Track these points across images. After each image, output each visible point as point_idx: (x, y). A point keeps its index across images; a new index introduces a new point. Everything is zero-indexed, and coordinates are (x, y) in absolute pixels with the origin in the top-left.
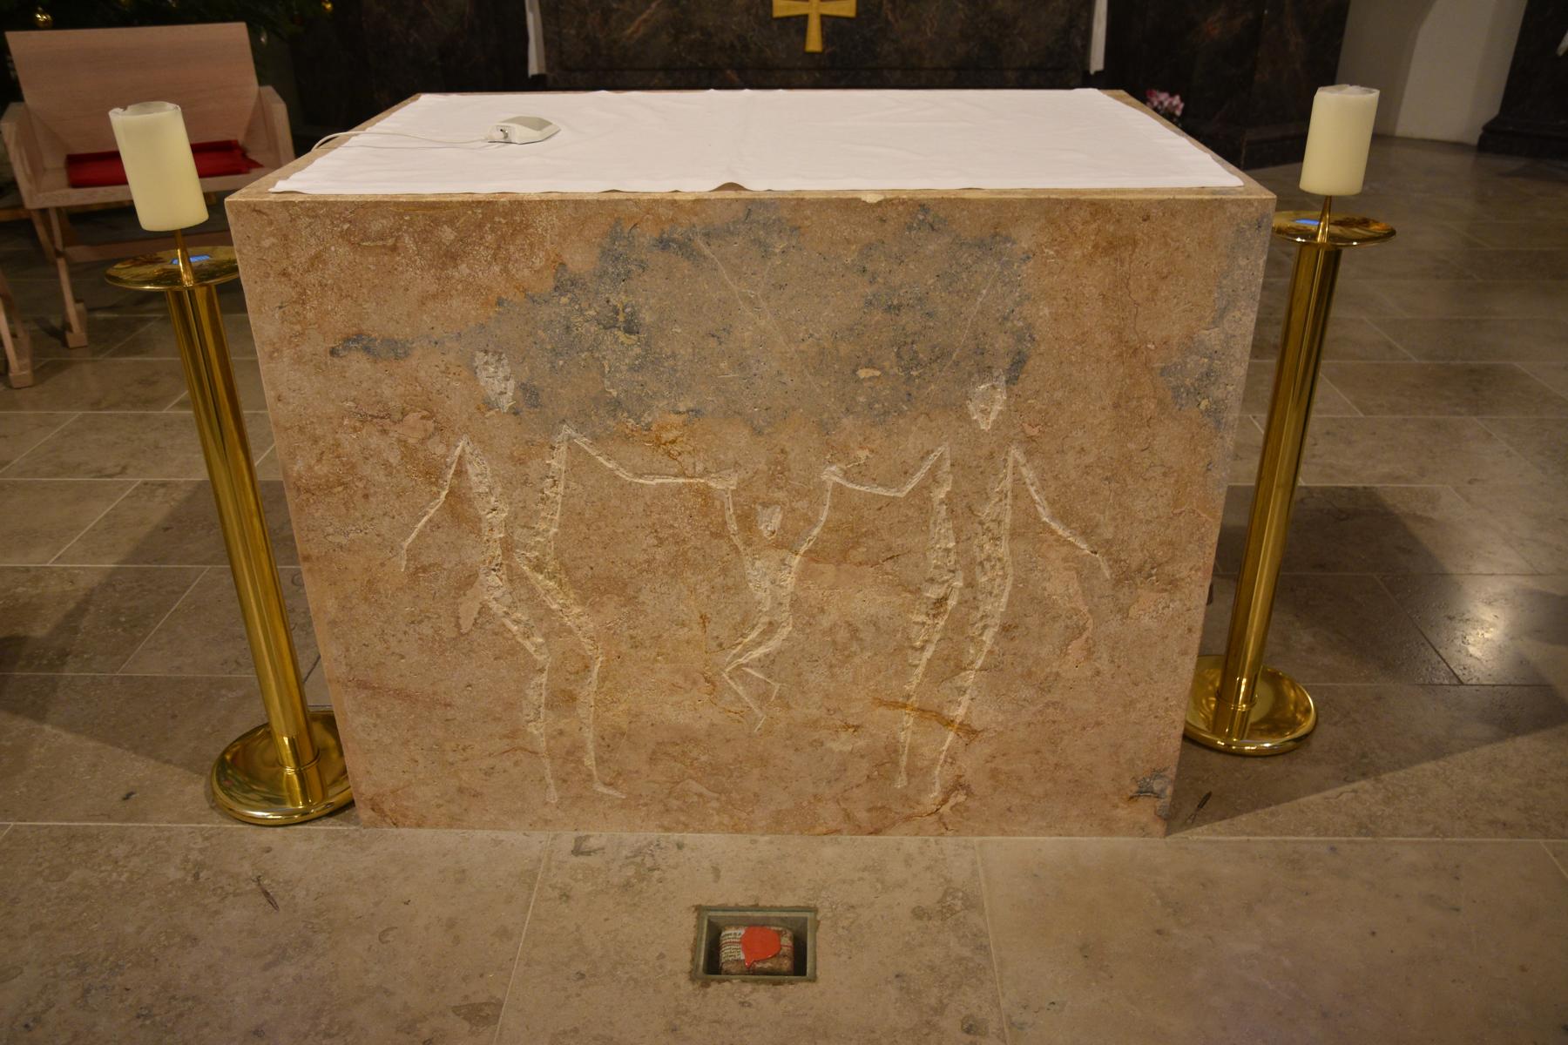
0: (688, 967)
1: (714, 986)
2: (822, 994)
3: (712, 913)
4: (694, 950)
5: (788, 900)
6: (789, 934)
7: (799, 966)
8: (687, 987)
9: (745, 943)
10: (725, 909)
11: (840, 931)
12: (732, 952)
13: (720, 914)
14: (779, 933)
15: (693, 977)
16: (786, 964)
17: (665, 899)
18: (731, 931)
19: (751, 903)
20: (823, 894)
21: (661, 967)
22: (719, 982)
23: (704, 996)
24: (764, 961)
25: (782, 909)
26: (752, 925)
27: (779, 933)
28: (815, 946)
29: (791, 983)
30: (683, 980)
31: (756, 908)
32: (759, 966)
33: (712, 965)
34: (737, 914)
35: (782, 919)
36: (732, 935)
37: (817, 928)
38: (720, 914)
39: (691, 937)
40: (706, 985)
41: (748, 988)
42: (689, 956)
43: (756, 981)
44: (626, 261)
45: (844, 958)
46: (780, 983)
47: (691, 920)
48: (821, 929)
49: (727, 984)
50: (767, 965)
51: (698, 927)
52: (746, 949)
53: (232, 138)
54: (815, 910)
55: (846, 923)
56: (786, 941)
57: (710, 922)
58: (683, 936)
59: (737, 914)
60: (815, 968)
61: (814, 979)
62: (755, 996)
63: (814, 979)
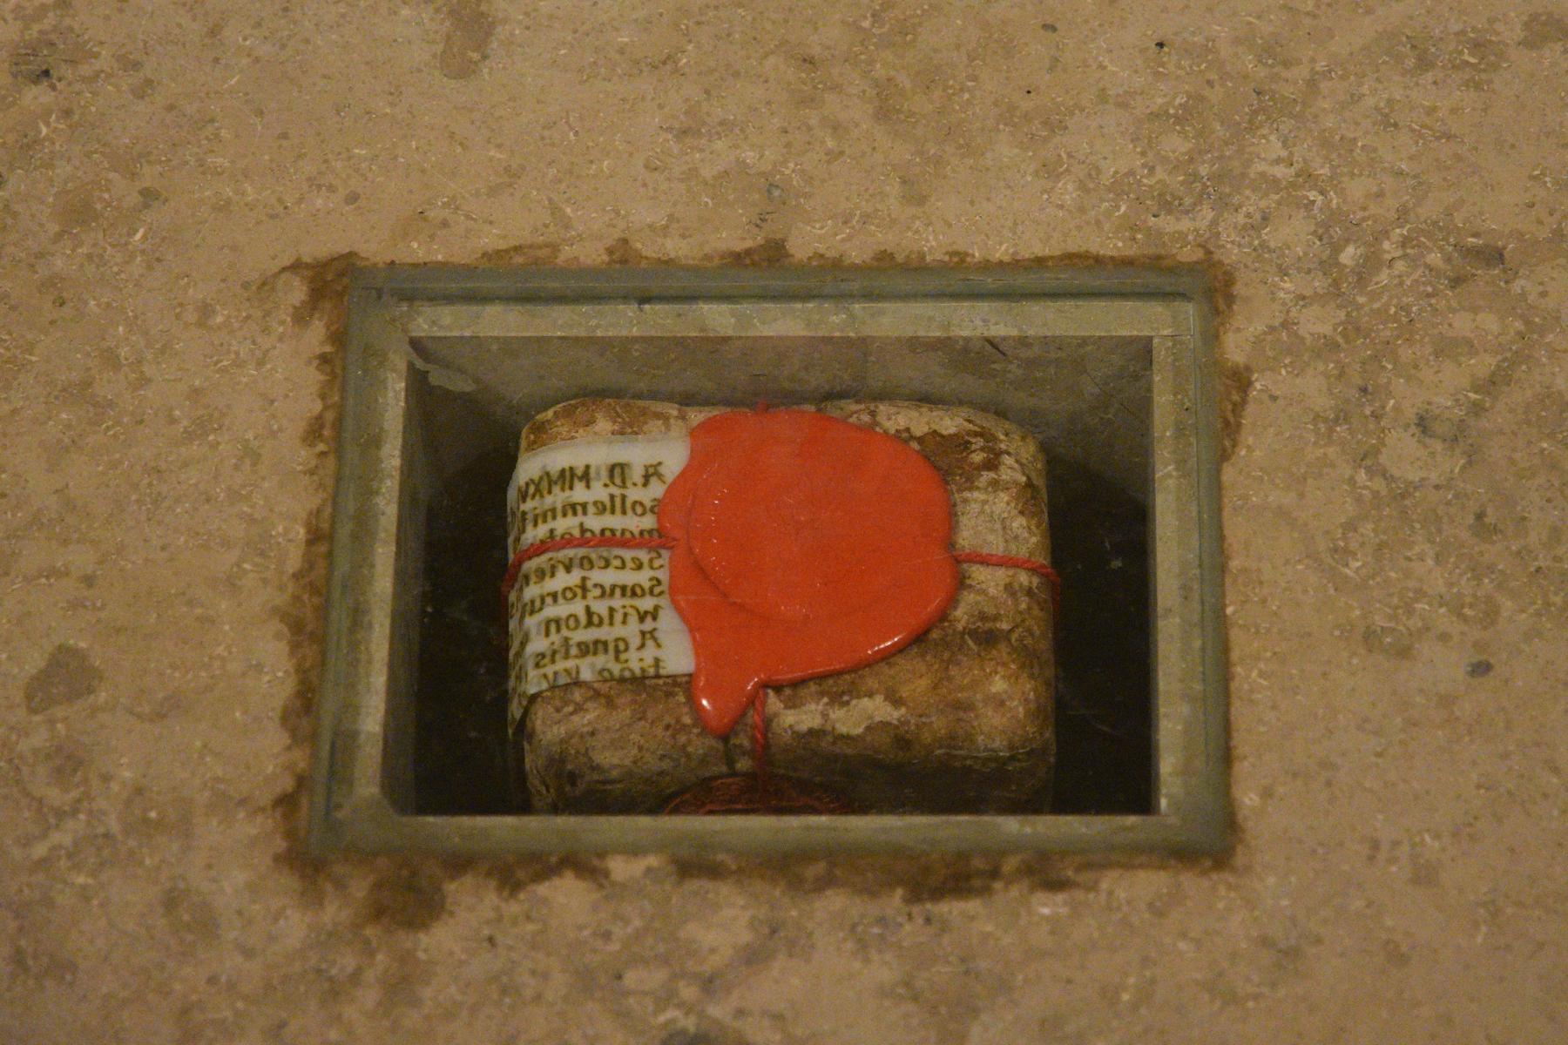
0: (269, 757)
1: (472, 905)
2: (1287, 957)
3: (440, 322)
4: (316, 624)
5: (1007, 209)
6: (1019, 459)
7: (1098, 742)
8: (269, 922)
9: (697, 546)
10: (528, 279)
11: (1405, 454)
12: (598, 627)
13: (499, 322)
14: (947, 462)
15: (309, 849)
16: (1002, 704)
17: (78, 213)
18: (585, 448)
19: (733, 236)
20: (1269, 153)
21: (68, 762)
22: (516, 872)
23: (402, 985)
24: (838, 681)
25: (959, 279)
26: (742, 398)
27: (947, 462)
28: (1215, 562)
29: (1045, 872)
30: (233, 867)
31: (764, 269)
32: (799, 717)
33: (460, 744)
34: (622, 322)
35: (980, 357)
36: (597, 475)
37: (1225, 433)
38: (499, 322)
39: (287, 508)
40: (409, 900)
41: (724, 921)
42: (272, 668)
43: (782, 866)
44: (708, 100)
45: (1442, 666)
46: (960, 877)
47: (280, 374)
48: (1258, 442)
49: (566, 895)
50: (860, 716)
51: (338, 433)
52: (706, 592)
53: (342, 248)
54: (1209, 287)
55: (1445, 387)
56: (998, 523)
57: (426, 399)
58: (225, 507)
59: (622, 322)
60: (1223, 757)
61: (1213, 845)
62: (781, 983)
63: (1213, 845)
